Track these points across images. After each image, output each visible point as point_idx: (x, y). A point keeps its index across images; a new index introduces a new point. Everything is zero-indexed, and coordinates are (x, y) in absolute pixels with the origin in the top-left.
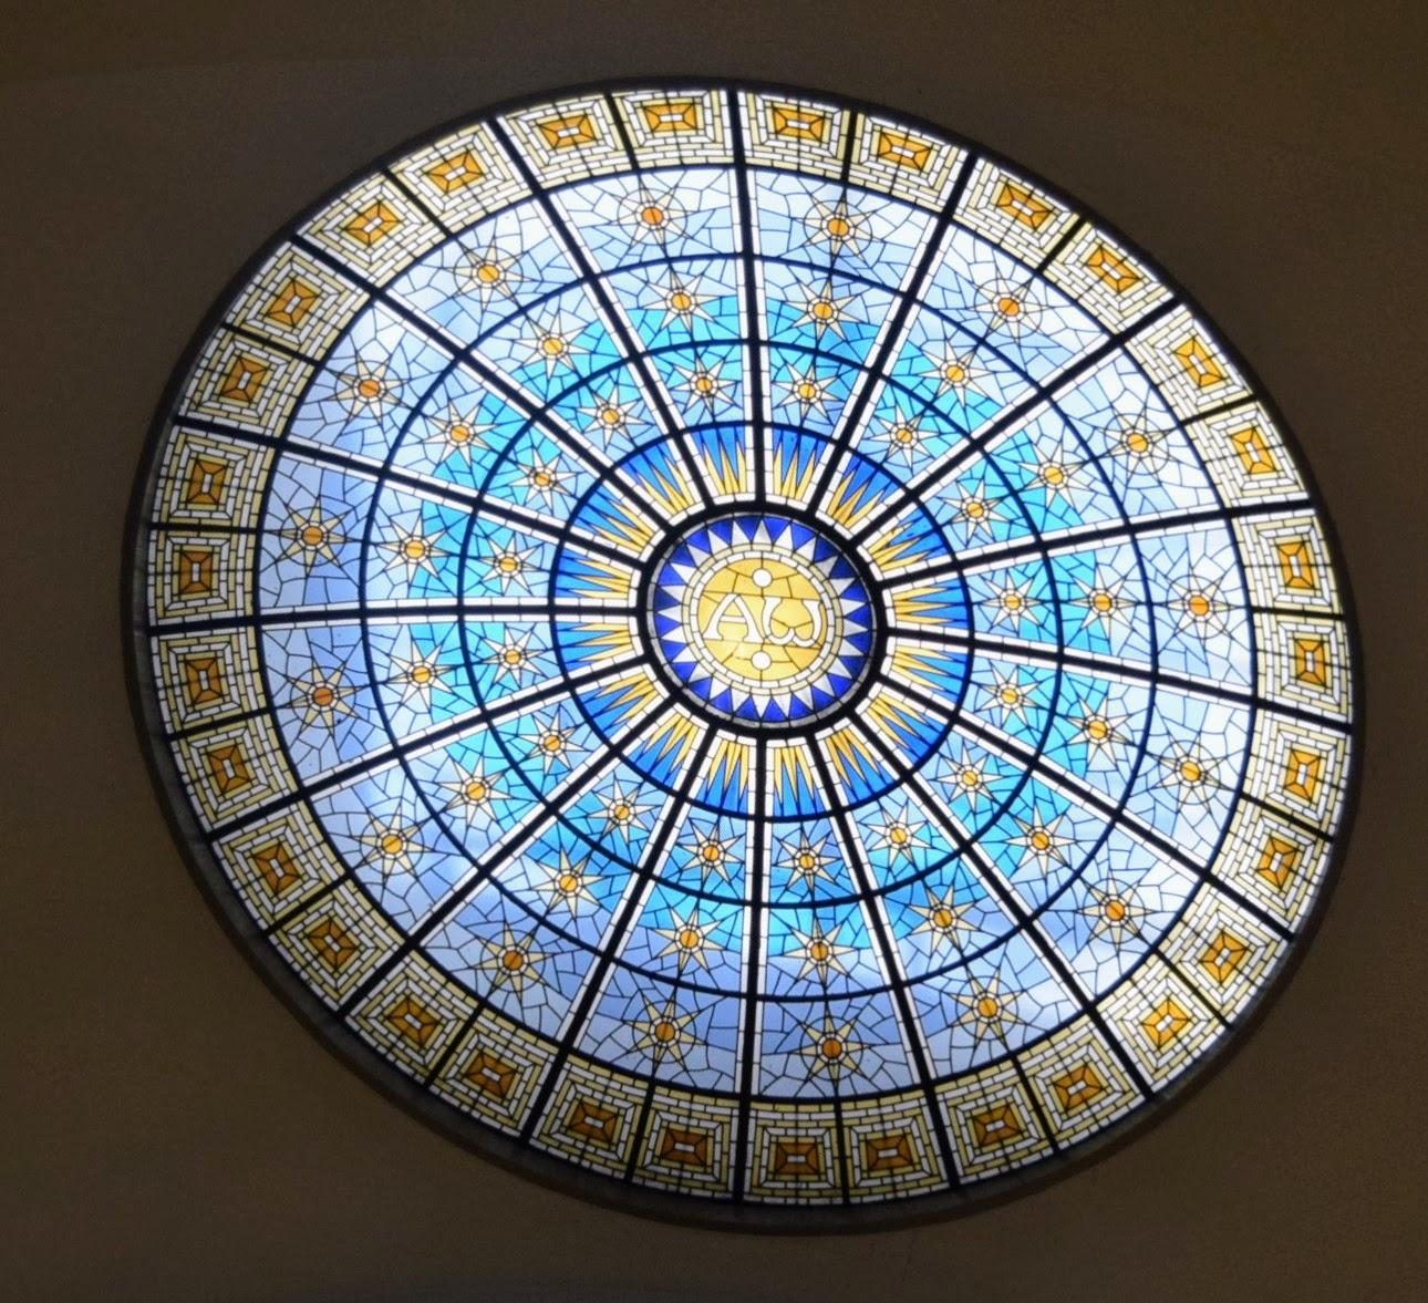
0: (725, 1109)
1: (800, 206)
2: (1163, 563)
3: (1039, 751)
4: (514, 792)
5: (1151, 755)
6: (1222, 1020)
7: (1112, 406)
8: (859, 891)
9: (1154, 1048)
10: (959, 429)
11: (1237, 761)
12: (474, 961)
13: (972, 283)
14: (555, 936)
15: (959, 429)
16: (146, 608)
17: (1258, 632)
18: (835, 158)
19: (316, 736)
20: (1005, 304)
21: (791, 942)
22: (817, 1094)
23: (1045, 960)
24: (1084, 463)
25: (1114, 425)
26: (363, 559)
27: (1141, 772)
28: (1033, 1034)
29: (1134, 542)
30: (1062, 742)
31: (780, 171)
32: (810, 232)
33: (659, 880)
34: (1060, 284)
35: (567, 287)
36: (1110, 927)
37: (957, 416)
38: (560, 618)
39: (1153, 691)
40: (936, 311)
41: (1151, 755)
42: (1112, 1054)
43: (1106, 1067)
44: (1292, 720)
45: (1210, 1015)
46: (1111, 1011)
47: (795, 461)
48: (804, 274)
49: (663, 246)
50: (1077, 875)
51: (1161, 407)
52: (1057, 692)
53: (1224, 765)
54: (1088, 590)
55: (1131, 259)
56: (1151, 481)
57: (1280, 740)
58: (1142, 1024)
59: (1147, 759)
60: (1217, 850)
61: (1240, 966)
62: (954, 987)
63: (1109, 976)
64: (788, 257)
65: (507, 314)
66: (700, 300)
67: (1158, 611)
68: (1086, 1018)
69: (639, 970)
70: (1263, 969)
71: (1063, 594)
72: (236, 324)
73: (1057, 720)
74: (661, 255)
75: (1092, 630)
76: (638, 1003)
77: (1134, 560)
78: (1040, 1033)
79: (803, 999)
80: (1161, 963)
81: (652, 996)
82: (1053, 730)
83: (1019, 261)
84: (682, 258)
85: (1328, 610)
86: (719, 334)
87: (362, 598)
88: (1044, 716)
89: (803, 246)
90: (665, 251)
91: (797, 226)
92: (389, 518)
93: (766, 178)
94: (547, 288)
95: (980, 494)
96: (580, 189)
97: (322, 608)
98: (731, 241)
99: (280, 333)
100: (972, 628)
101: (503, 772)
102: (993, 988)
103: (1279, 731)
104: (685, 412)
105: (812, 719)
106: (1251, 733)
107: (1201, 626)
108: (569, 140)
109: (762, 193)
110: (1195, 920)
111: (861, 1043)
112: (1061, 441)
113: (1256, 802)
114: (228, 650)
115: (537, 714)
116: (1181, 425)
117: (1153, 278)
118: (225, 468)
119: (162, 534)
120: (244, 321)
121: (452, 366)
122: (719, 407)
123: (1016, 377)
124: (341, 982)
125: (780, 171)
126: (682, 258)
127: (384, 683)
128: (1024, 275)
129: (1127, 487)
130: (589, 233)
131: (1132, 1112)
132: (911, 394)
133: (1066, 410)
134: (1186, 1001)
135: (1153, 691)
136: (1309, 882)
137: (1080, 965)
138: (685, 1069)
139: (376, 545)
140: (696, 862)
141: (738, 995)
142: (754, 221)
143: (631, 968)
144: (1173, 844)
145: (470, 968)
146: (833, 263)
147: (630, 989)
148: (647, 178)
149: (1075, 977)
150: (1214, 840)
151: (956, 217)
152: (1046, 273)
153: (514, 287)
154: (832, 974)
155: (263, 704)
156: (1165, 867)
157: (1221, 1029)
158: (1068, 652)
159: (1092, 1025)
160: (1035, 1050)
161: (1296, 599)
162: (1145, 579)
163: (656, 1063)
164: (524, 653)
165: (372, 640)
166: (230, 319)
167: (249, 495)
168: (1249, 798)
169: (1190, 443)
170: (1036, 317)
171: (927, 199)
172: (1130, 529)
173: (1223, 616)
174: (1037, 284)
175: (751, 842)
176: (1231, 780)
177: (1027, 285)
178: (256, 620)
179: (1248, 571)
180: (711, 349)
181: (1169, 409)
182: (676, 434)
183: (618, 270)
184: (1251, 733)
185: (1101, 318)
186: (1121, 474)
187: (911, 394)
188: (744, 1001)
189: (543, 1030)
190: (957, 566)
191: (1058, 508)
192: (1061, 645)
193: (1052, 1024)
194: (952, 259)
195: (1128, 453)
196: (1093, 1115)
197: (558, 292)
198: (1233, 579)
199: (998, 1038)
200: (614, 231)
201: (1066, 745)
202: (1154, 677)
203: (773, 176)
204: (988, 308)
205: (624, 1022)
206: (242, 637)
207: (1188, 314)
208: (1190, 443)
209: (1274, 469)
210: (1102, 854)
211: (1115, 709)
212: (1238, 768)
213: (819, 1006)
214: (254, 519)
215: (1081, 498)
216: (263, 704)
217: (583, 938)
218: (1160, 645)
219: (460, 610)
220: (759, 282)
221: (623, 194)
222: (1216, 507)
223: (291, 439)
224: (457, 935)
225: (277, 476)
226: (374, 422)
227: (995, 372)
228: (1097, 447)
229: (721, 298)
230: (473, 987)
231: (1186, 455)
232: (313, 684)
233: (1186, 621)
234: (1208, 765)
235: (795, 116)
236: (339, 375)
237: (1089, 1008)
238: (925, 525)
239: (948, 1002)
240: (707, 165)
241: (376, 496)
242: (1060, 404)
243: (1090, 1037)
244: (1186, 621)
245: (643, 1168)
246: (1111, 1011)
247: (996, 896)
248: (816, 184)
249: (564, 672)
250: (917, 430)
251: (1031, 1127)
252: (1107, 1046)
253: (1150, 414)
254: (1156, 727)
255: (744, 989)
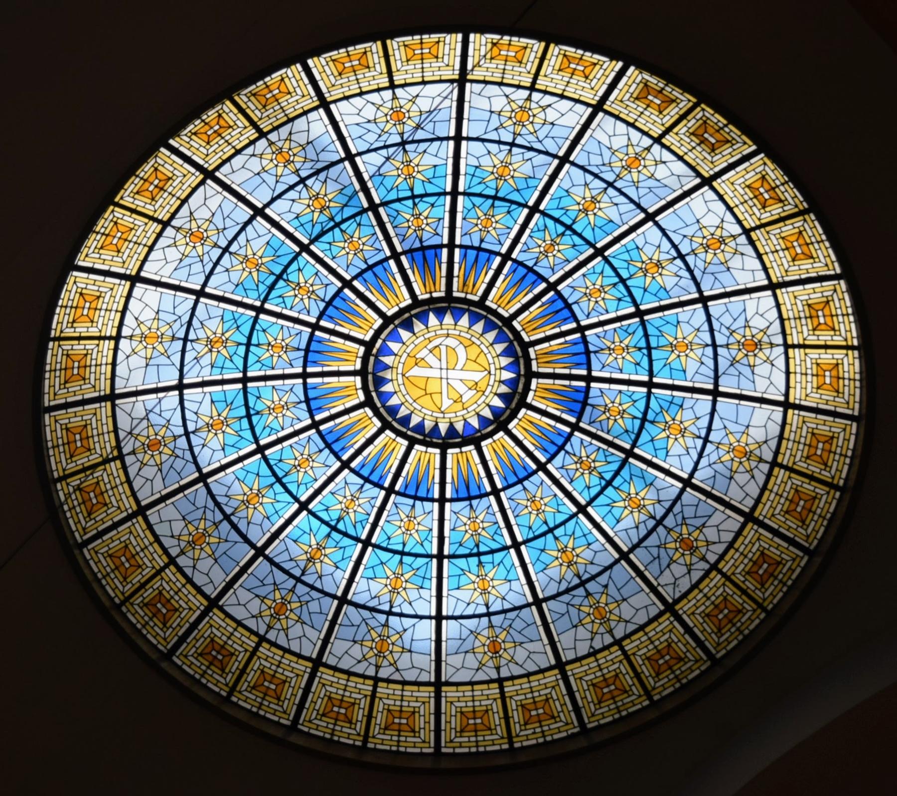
0: (666, 621)
1: (255, 165)
2: (596, 160)
3: (636, 305)
4: (415, 566)
5: (688, 254)
6: (852, 348)
7: (492, 112)
8: (623, 456)
9: (835, 394)
10: (439, 194)
11: (729, 217)
12: (476, 665)
13: (369, 121)
14: (503, 616)
15: (439, 194)
16: (155, 647)
17: (673, 147)
18: (245, 128)
19: (296, 631)
20: (395, 116)
21: (617, 512)
22: (701, 573)
23: (742, 402)
24: (510, 151)
25: (503, 119)
26: (235, 527)
27: (692, 266)
28: (773, 444)
29: (573, 164)
30: (642, 290)
31: (229, 159)
32: (273, 171)
33: (525, 542)
34: (408, 81)
35: (194, 309)
36: (755, 355)
37: (431, 189)
38: (353, 465)
39: (657, 224)
40: (369, 151)
41: (688, 254)
42: (819, 416)
43: (825, 426)
44: (732, 173)
45: (844, 351)
46: (798, 396)
47: (427, 268)
48: (292, 194)
49: (216, 245)
50: (714, 346)
51: (513, 89)
52: (614, 269)
53: (725, 225)
54: (576, 207)
55: (424, 36)
56: (548, 127)
57: (738, 187)
58: (818, 388)
59: (688, 258)
60: (765, 269)
61: (834, 313)
62: (714, 457)
63: (779, 379)
64: (276, 193)
65: (180, 348)
66: (260, 254)
67: (618, 184)
68: (790, 412)
69: (559, 594)
70: (843, 303)
71: (568, 222)
72: (61, 474)
73: (629, 283)
74: (220, 251)
75: (599, 224)
76: (573, 611)
77: (581, 172)
78: (776, 440)
79: (649, 533)
80: (797, 350)
81: (577, 601)
82: (632, 289)
83: (378, 90)
84: (230, 243)
85: (691, 104)
86: (285, 261)
87: (253, 545)
88: (621, 287)
89: (277, 182)
90: (220, 247)
91: (264, 175)
92: (226, 496)
93: (226, 169)
94: (186, 318)
95: (480, 214)
96: (150, 258)
97: (237, 569)
98: (245, 213)
99: (86, 459)
100: (544, 280)
101: (401, 562)
102: (732, 440)
103: (732, 184)
104: (308, 312)
105: (517, 397)
106: (721, 198)
107: (645, 171)
108: (121, 241)
109: (231, 177)
110: (791, 313)
111: (698, 528)
112: (489, 152)
113: (758, 227)
114: (214, 631)
115: (388, 519)
116: (532, 88)
117: (444, 35)
118: (126, 546)
119: (653, 693)
120: (64, 470)
121: (181, 396)
122: (321, 293)
123: (436, 144)
124: (422, 736)
125: (229, 159)
126: (230, 243)
127: (303, 574)
128: (387, 95)
129: (541, 142)
130: (175, 275)
131: (857, 435)
132: (399, 200)
133: (475, 136)
134: (827, 357)
135: (657, 224)
136: (822, 241)
137: (761, 388)
138: (627, 622)
139: (233, 514)
140: (533, 517)
141: (617, 562)
142: (243, 193)
143: (553, 597)
144: (742, 287)
145: (477, 670)
146: (299, 176)
147: (562, 608)
148: (174, 223)
149: (765, 396)
150: (758, 266)
151: (329, 99)
152: (396, 83)
153: (170, 333)
154: (650, 508)
155: (496, 685)
156: (751, 302)
157: (856, 353)
158: (599, 245)
159: (796, 412)
160: (782, 450)
161: (672, 114)
162: (596, 176)
163: (610, 632)
164: (354, 498)
165: (277, 560)
166: (56, 475)
167: (150, 548)
168: (753, 229)
169: (545, 92)
170: (415, 108)
171: (308, 104)
172: (564, 160)
173: (649, 156)
174: (399, 92)
175: (549, 482)
176: (737, 230)
177: (394, 97)
178: (213, 603)
179: (637, 124)
180: (289, 271)
181: (519, 87)
182: (315, 327)
183: (208, 278)
184: (721, 198)
185: (443, 78)
186: (531, 138)
187: (399, 200)
188: (623, 562)
189: (542, 667)
190: (506, 257)
191: (522, 185)
192: (592, 245)
193: (776, 430)
194: (349, 120)
195: (523, 126)
196: (841, 455)
197: (193, 315)
198: (635, 135)
199: (759, 462)
200: (187, 261)
201: (645, 290)
202: (650, 217)
203: (228, 165)
204: (389, 126)
205: (576, 626)
206: (215, 618)
207: (478, 35)
208: (545, 92)
209: (595, 64)
210: (716, 325)
211: (649, 250)
212: (733, 220)
213: (660, 529)
214: (164, 557)
215: (527, 169)
216: (256, 639)
217: (326, 589)
218: (636, 199)
219: (304, 506)
220: (277, 218)
221: (173, 241)
222: (590, 110)
223: (143, 503)
224: (456, 660)
225: (155, 527)
226: (173, 458)
227: (425, 151)
228: (508, 137)
229: (268, 243)
230: (488, 678)
231: (548, 99)
232: (270, 608)
233: (635, 176)
234: (718, 232)
235: (207, 127)
236: (133, 452)
237: (786, 405)
238: (472, 254)
239: (719, 467)
240: (194, 190)
241: (209, 491)
242: (470, 136)
243: (801, 418)
244: (635, 176)
245: (654, 688)
246: (798, 396)
247: (688, 395)
248: (251, 148)
249: (381, 487)
250: (420, 214)
251: (817, 490)
252: (813, 415)
253: (512, 97)
254: (676, 239)
255: (617, 556)
